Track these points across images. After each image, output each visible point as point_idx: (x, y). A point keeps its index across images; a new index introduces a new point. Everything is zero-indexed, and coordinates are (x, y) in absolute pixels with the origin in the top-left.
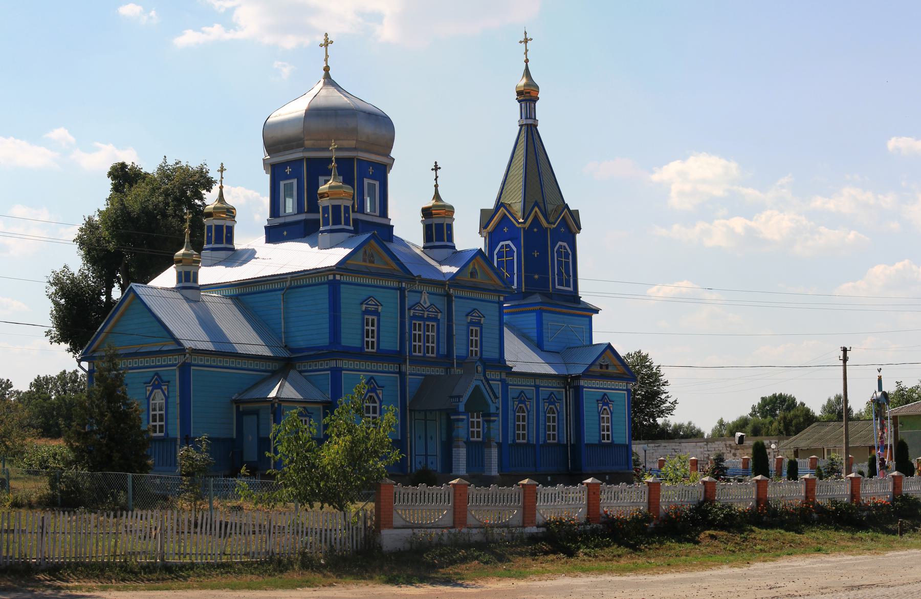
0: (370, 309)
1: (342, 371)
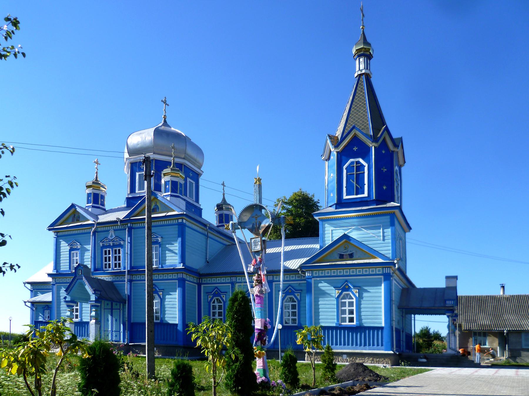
0: (115, 244)
1: (201, 285)
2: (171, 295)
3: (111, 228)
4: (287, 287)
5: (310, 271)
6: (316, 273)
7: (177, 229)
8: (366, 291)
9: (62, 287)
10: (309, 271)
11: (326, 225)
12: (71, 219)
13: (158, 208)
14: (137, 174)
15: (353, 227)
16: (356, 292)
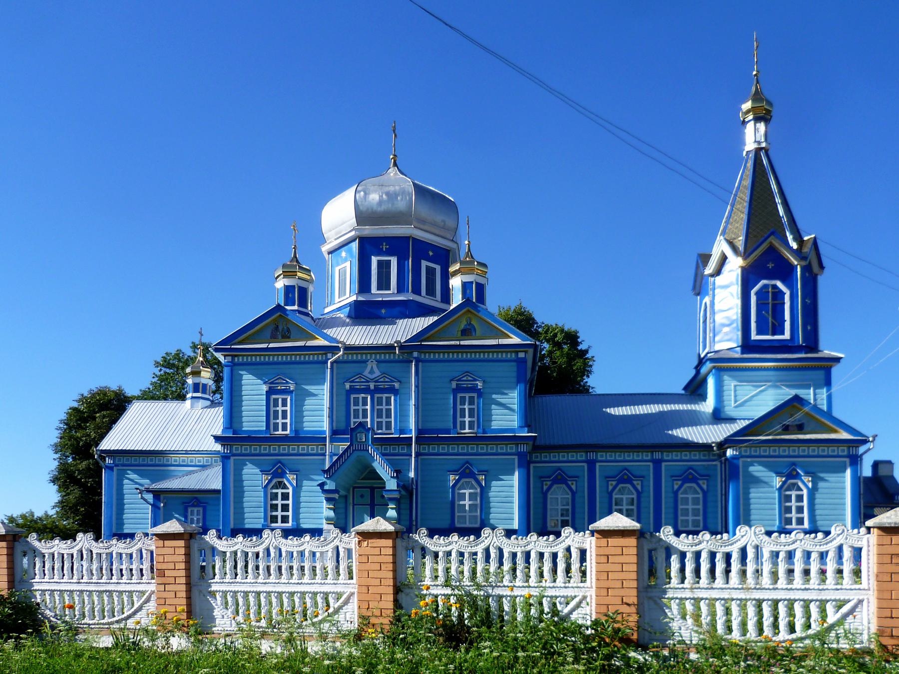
2: (502, 480)
3: (369, 358)
4: (622, 471)
5: (227, 445)
6: (237, 449)
7: (515, 369)
8: (823, 479)
9: (247, 463)
10: (226, 446)
11: (726, 377)
12: (268, 333)
13: (475, 330)
14: (374, 260)
15: (769, 384)
16: (809, 481)
